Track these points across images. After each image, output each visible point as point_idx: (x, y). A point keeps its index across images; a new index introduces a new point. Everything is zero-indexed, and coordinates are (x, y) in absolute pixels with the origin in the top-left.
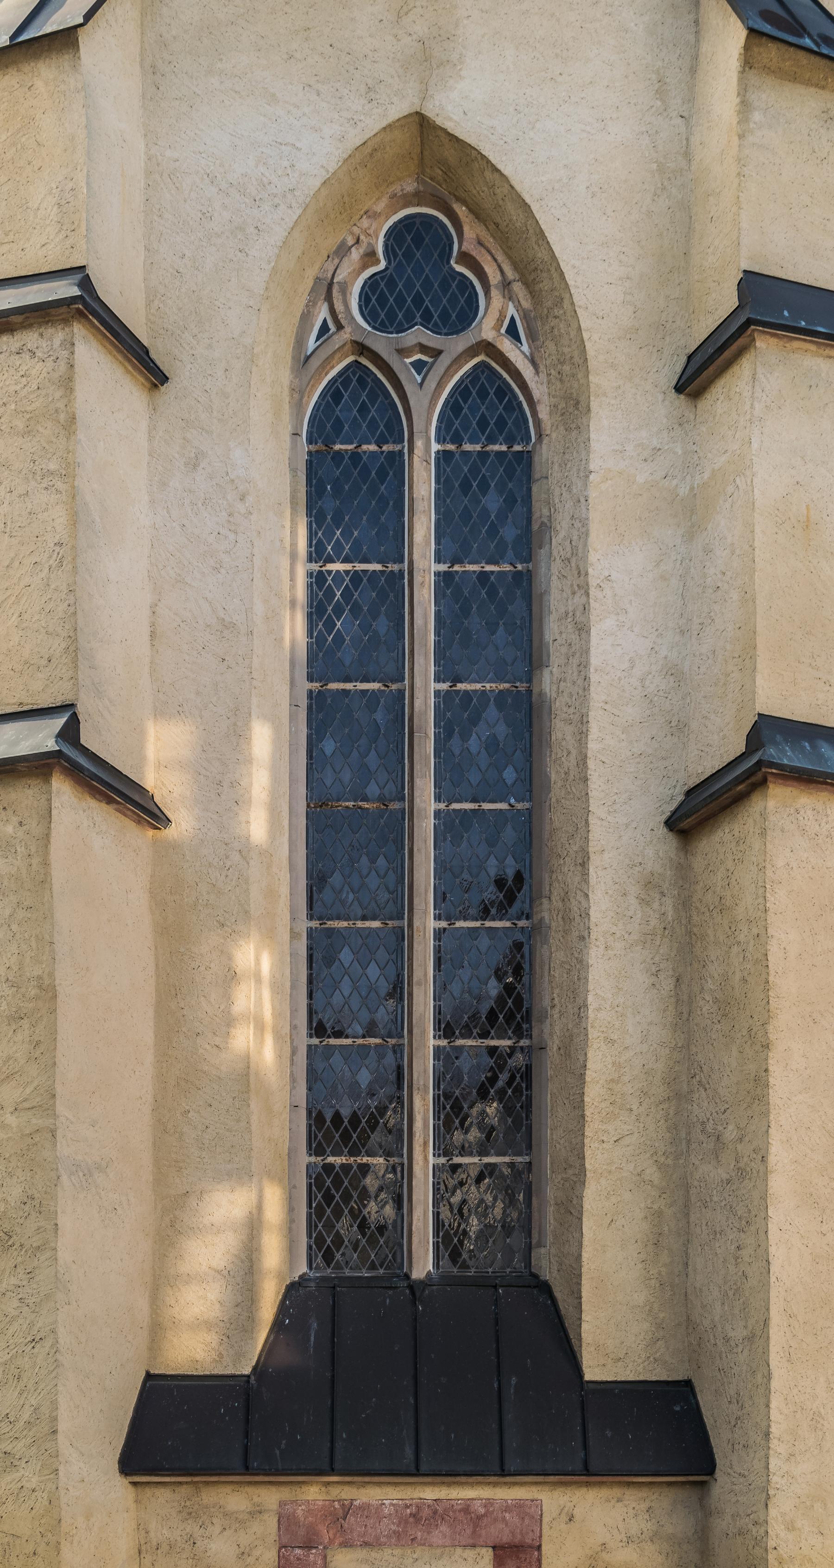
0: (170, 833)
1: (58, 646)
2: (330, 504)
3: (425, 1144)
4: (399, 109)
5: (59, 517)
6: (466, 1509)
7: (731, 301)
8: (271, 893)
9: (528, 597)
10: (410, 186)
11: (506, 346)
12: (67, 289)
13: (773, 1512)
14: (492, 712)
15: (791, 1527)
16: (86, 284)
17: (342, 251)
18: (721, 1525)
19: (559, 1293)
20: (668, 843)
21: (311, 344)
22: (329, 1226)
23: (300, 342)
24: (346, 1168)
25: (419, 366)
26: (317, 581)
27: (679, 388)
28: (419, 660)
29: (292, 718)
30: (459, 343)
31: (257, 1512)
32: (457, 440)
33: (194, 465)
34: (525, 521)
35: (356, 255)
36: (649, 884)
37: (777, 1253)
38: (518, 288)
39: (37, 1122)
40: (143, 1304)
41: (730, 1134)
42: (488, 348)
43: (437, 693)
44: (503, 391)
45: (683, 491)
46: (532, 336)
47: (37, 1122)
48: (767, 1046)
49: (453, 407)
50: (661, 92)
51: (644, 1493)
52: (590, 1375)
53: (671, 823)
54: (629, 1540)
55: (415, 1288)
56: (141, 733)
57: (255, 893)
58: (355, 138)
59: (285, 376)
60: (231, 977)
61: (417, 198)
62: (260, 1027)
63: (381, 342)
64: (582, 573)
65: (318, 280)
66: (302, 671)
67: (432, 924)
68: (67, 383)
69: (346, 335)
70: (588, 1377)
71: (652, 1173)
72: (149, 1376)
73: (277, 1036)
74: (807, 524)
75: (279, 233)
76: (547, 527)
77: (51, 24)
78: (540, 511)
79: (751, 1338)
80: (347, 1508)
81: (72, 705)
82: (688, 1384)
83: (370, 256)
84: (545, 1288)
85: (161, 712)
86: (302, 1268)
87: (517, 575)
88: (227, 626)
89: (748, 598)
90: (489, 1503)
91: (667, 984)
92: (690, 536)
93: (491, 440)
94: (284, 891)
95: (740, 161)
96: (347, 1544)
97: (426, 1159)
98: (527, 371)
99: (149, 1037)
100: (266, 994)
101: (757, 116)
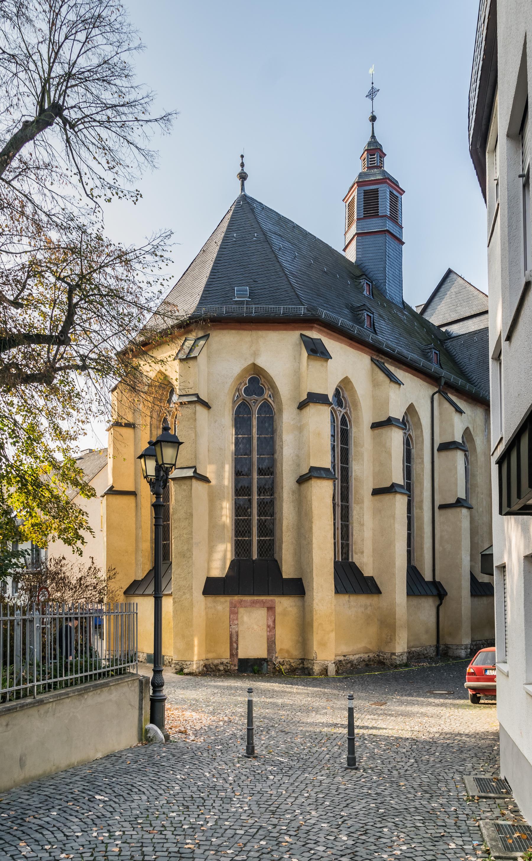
0: (211, 484)
1: (193, 456)
2: (238, 425)
4: (250, 362)
5: (193, 435)
6: (262, 601)
7: (306, 397)
8: (228, 493)
9: (273, 441)
10: (252, 373)
11: (269, 399)
12: (195, 399)
13: (314, 602)
14: (267, 461)
16: (198, 397)
17: (241, 384)
18: (306, 604)
20: (297, 485)
21: (235, 399)
22: (238, 550)
23: (234, 398)
24: (241, 540)
25: (254, 402)
26: (237, 439)
27: (298, 408)
28: (254, 453)
29: (232, 462)
30: (262, 398)
31: (226, 601)
32: (261, 414)
33: (215, 422)
35: (243, 384)
36: (293, 492)
37: (314, 558)
38: (271, 389)
39: (189, 536)
40: (206, 565)
41: (307, 536)
42: (266, 399)
44: (268, 406)
45: (299, 425)
46: (273, 397)
47: (189, 536)
48: (312, 522)
49: (260, 409)
50: (295, 359)
51: (293, 598)
52: (285, 576)
53: (297, 482)
54: (291, 606)
56: (206, 467)
57: (226, 494)
58: (243, 367)
59: (231, 405)
60: (222, 508)
61: (254, 374)
62: (227, 517)
63: (247, 398)
64: (282, 439)
65: (236, 389)
66: (234, 454)
68: (195, 413)
69: (241, 397)
70: (285, 576)
71: (294, 542)
72: (207, 577)
73: (229, 518)
74: (319, 434)
75: (230, 383)
76: (276, 430)
78: (275, 426)
79: (310, 572)
80: (241, 601)
82: (301, 579)
83: (246, 384)
84: (276, 561)
85: (210, 463)
86: (234, 558)
87: (271, 437)
88: (221, 449)
89: (309, 447)
90: (266, 600)
91: (297, 509)
92: (300, 433)
93: (266, 414)
94: (231, 492)
95: (307, 374)
96: (242, 607)
98: (272, 403)
99: (207, 519)
100: (228, 511)
101: (310, 366)
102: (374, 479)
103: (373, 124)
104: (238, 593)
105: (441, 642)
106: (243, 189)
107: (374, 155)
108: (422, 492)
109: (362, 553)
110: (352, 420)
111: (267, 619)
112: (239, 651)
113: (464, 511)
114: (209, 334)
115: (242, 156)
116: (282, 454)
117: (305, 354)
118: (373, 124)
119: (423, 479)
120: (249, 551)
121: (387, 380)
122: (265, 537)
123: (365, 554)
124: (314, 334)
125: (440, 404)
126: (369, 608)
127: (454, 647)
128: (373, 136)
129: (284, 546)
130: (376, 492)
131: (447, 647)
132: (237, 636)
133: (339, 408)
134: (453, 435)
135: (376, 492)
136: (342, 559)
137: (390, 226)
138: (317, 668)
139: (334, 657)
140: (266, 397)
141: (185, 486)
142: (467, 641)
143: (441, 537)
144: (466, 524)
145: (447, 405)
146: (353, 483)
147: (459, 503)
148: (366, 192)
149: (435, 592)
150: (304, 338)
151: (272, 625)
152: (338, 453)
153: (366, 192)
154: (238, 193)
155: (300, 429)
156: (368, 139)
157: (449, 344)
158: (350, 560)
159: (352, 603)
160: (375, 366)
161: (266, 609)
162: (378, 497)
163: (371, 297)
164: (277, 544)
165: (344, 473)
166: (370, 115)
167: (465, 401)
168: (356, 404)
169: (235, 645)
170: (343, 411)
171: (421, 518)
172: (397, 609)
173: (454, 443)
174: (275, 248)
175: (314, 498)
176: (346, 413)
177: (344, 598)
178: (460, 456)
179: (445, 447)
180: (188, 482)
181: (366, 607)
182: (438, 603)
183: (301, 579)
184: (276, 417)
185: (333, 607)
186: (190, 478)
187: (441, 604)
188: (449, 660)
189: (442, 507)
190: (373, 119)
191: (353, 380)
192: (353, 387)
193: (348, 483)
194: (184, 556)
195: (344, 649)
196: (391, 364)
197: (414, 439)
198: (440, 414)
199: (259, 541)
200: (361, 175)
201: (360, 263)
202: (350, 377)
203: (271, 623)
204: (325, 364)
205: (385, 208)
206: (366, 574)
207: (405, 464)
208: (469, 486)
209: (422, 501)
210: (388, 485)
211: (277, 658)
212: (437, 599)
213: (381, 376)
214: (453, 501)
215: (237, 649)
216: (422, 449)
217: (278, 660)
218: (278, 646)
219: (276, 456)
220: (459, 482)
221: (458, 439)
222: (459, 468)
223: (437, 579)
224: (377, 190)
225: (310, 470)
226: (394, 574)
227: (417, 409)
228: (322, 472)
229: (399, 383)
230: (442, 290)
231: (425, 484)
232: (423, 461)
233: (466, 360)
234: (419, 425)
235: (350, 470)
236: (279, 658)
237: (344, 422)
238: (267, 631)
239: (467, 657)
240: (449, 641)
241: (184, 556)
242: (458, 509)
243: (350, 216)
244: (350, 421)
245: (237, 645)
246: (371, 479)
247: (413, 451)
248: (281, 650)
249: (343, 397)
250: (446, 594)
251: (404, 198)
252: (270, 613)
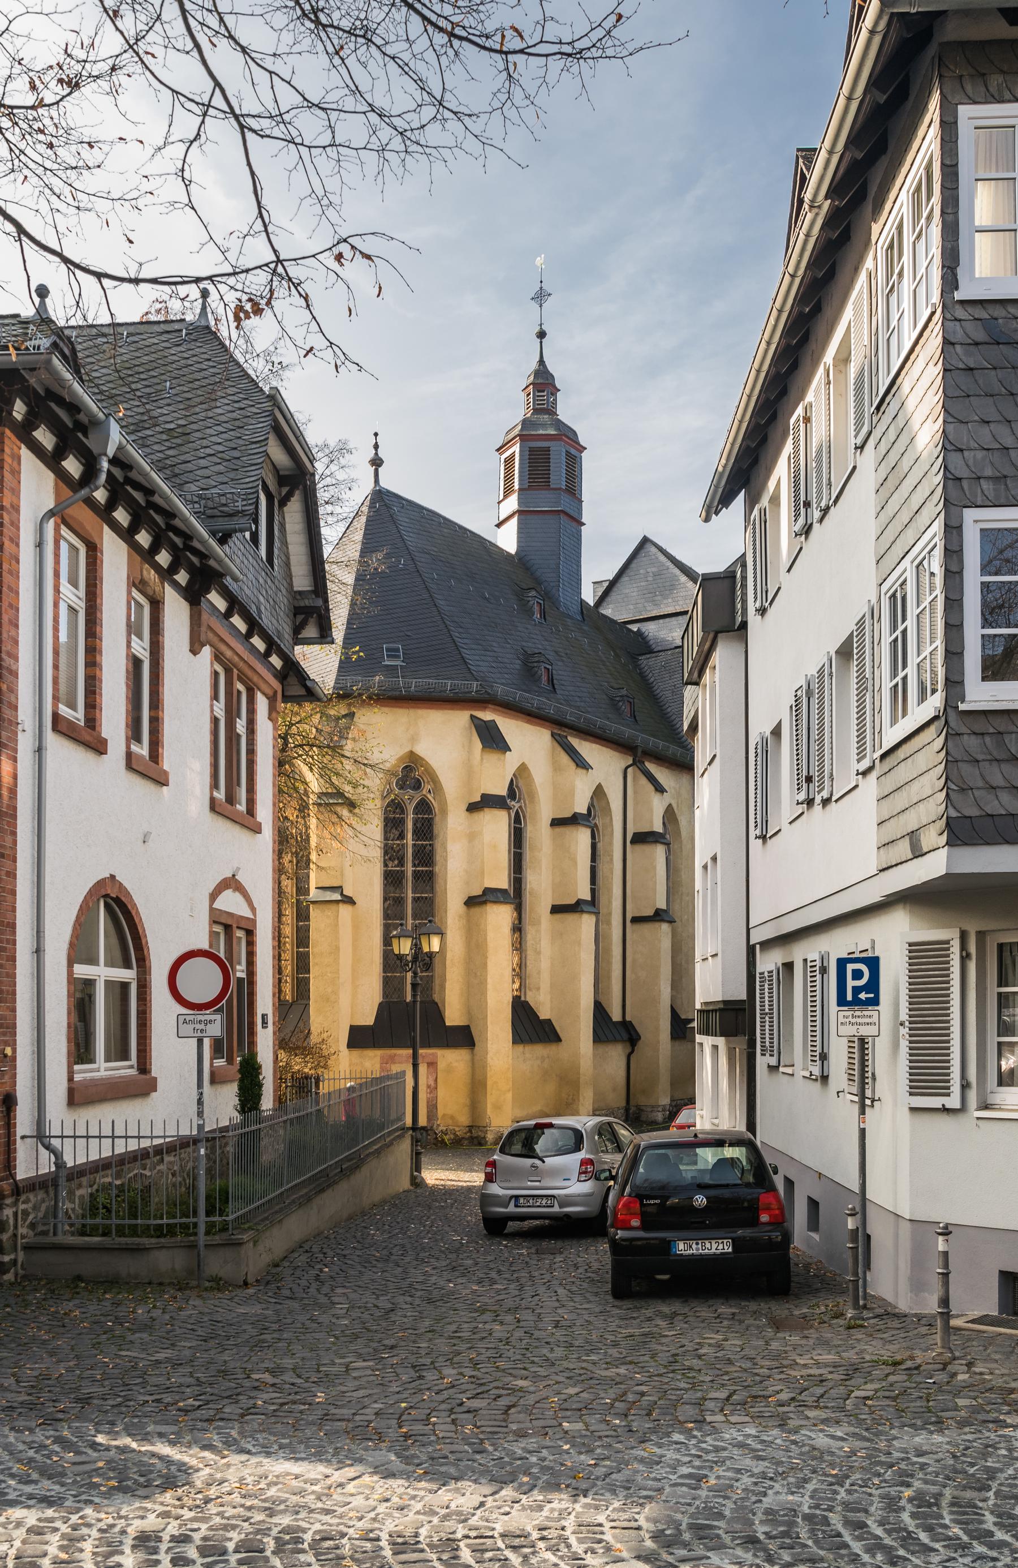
4: (407, 750)
11: (428, 796)
20: (464, 908)
31: (375, 1056)
34: (533, 1122)
36: (460, 917)
37: (489, 1001)
44: (427, 804)
49: (416, 807)
55: (407, 1004)
64: (445, 849)
81: (341, 887)
82: (468, 1026)
84: (436, 1004)
89: (483, 862)
102: (553, 892)
103: (541, 343)
104: (393, 1046)
105: (632, 1102)
106: (377, 481)
107: (543, 391)
108: (610, 902)
109: (538, 989)
110: (528, 815)
113: (665, 927)
114: (354, 713)
115: (376, 434)
116: (446, 868)
117: (478, 745)
118: (541, 343)
119: (612, 884)
120: (401, 990)
121: (573, 765)
123: (541, 991)
124: (487, 715)
125: (635, 778)
126: (547, 1060)
127: (649, 1109)
128: (541, 361)
129: (448, 985)
130: (557, 909)
131: (639, 1109)
134: (651, 822)
135: (557, 909)
138: (490, 1137)
139: (509, 1123)
140: (424, 792)
141: (329, 911)
142: (665, 1101)
143: (634, 961)
144: (666, 944)
145: (644, 781)
147: (659, 916)
148: (532, 450)
149: (625, 1036)
150: (476, 721)
151: (433, 1085)
153: (532, 450)
155: (472, 837)
156: (534, 365)
157: (644, 661)
159: (527, 1055)
160: (556, 745)
162: (558, 916)
164: (437, 982)
165: (517, 886)
166: (537, 329)
167: (667, 768)
168: (533, 796)
170: (517, 806)
172: (582, 1062)
173: (653, 834)
175: (489, 927)
176: (520, 807)
177: (520, 1048)
178: (659, 852)
179: (643, 838)
180: (333, 907)
181: (543, 1059)
182: (629, 1050)
183: (468, 1026)
184: (437, 819)
185: (510, 1061)
186: (337, 902)
187: (632, 1052)
188: (642, 1126)
189: (636, 920)
190: (542, 335)
194: (328, 1000)
195: (519, 1113)
196: (575, 736)
197: (601, 829)
198: (635, 792)
200: (525, 423)
201: (523, 554)
203: (432, 1083)
204: (502, 757)
205: (558, 477)
206: (542, 1017)
208: (671, 884)
210: (573, 901)
211: (439, 1125)
212: (628, 1044)
213: (565, 759)
214: (650, 912)
216: (611, 843)
217: (440, 1128)
218: (441, 1112)
220: (658, 887)
221: (658, 827)
222: (658, 868)
223: (628, 1019)
224: (548, 449)
225: (484, 892)
226: (579, 1017)
228: (499, 895)
230: (633, 565)
231: (614, 891)
232: (612, 860)
233: (668, 694)
234: (607, 810)
235: (523, 880)
236: (441, 1125)
237: (517, 819)
239: (664, 1122)
240: (642, 1101)
241: (328, 1000)
242: (657, 925)
243: (508, 478)
244: (524, 817)
246: (550, 893)
248: (444, 1115)
249: (517, 786)
250: (639, 1037)
252: (431, 1070)
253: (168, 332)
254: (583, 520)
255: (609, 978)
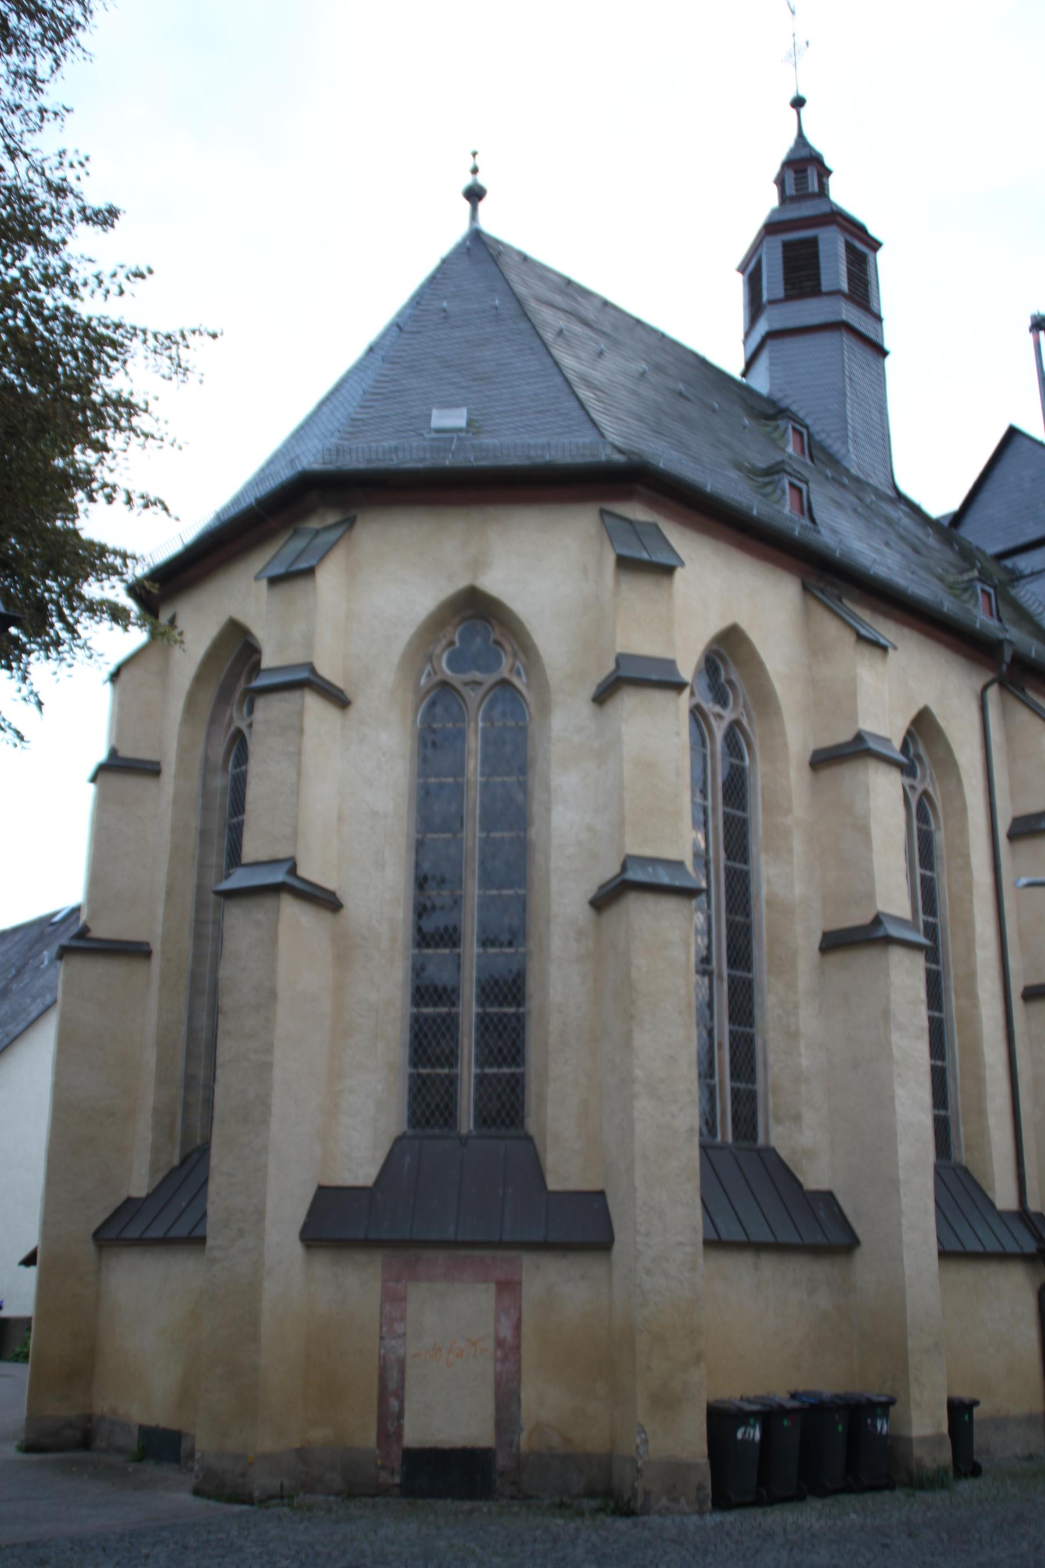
3: (469, 1063)
4: (462, 583)
15: (648, 1272)
19: (537, 1141)
24: (429, 1075)
38: (521, 654)
43: (480, 839)
46: (527, 674)
52: (553, 1184)
67: (474, 1070)
70: (553, 1184)
72: (321, 1189)
77: (303, 565)
82: (601, 1193)
97: (474, 834)
108: (970, 951)
109: (797, 1118)
111: (497, 1320)
112: (408, 1422)
122: (500, 1066)
125: (1005, 714)
132: (402, 1372)
133: (717, 709)
136: (736, 1137)
137: (849, 313)
146: (762, 916)
152: (715, 828)
154: (457, 231)
158: (761, 1140)
161: (493, 1287)
163: (808, 461)
169: (394, 1403)
170: (729, 715)
171: (972, 1020)
174: (549, 336)
183: (601, 1193)
191: (755, 636)
192: (753, 655)
193: (748, 915)
199: (481, 1080)
202: (744, 625)
203: (507, 1333)
207: (919, 871)
209: (971, 976)
215: (400, 1415)
216: (963, 831)
219: (533, 833)
223: (1034, 1205)
224: (814, 242)
227: (942, 723)
229: (882, 648)
234: (947, 764)
235: (753, 877)
238: (497, 1360)
244: (749, 745)
245: (402, 1402)
247: (940, 838)
251: (883, 259)
253: (403, 432)
254: (887, 345)
255: (981, 1112)
